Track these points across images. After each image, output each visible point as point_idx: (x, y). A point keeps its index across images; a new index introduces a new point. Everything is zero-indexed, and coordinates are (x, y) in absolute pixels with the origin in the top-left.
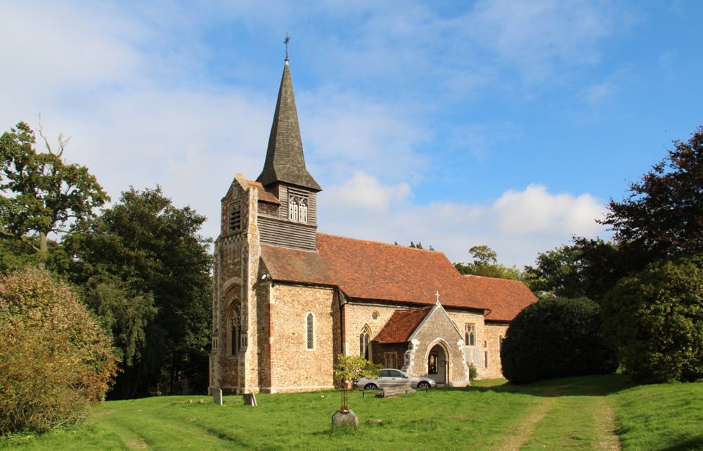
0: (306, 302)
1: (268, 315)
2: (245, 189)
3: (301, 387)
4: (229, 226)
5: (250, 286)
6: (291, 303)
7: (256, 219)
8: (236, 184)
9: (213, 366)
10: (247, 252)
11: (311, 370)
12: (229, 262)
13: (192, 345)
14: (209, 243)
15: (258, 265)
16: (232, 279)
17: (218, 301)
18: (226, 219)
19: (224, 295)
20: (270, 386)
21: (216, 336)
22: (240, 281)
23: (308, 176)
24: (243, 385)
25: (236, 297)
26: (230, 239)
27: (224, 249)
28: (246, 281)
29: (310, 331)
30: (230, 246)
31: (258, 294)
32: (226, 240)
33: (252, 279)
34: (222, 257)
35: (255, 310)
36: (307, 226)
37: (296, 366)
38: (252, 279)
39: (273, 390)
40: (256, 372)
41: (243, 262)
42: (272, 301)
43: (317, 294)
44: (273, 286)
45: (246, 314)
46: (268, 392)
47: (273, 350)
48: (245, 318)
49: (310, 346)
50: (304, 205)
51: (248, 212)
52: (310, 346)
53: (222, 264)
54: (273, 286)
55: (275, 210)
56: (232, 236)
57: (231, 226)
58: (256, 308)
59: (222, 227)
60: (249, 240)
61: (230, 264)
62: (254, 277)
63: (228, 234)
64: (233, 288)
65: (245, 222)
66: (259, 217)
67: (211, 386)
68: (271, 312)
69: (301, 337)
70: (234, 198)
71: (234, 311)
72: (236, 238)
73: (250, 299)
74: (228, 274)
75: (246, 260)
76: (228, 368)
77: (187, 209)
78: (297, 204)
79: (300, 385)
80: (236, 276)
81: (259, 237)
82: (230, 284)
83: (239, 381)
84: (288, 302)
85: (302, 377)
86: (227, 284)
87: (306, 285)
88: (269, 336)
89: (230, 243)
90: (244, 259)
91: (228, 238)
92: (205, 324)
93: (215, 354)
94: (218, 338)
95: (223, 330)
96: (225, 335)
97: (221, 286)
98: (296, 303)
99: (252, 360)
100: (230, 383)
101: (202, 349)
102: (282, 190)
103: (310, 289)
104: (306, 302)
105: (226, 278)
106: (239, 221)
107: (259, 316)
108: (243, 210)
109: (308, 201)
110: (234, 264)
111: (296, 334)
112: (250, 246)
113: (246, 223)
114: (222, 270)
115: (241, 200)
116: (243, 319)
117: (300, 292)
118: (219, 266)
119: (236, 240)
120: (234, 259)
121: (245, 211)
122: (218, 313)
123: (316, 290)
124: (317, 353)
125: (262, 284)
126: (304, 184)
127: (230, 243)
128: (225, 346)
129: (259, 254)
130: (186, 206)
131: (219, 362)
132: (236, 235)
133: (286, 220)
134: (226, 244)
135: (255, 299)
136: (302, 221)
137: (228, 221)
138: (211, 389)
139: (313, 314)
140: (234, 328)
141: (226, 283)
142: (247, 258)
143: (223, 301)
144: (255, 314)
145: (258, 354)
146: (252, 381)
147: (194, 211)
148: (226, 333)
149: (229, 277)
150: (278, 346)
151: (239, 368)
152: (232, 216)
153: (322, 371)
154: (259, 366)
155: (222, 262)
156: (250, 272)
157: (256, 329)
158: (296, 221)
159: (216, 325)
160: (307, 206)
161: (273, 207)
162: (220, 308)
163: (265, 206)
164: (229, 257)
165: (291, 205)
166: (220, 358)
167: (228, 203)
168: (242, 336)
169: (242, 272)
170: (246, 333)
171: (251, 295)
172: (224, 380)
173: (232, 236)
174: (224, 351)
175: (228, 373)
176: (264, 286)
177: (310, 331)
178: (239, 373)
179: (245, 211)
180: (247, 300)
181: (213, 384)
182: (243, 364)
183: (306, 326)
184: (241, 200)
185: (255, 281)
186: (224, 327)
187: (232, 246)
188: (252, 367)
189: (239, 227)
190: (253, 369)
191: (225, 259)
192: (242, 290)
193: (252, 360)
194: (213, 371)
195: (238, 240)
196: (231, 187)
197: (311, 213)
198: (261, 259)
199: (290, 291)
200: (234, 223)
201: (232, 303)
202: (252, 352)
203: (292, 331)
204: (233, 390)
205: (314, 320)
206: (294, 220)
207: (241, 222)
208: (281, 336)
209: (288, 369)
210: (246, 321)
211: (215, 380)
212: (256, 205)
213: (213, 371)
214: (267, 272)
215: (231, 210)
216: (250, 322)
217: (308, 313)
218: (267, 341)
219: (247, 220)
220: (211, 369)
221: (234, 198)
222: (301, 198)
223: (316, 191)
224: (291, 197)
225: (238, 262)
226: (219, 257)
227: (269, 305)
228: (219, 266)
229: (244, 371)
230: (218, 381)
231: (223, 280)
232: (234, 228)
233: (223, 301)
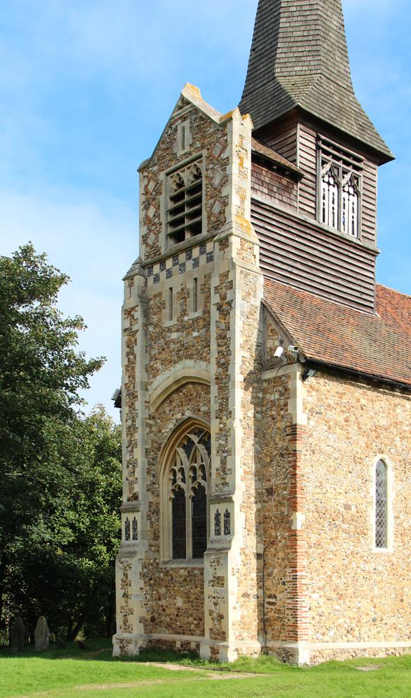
0: (376, 428)
1: (290, 455)
2: (216, 118)
3: (362, 645)
4: (165, 230)
5: (239, 378)
6: (342, 428)
7: (248, 206)
8: (186, 111)
9: (126, 583)
10: (231, 286)
11: (383, 601)
12: (167, 323)
13: (43, 542)
14: (74, 330)
15: (256, 325)
16: (179, 366)
17: (138, 423)
18: (157, 215)
19: (152, 410)
20: (295, 638)
21: (134, 510)
22: (206, 370)
23: (360, 113)
24: (222, 635)
25: (188, 414)
26: (169, 263)
27: (150, 294)
28: (225, 364)
29: (381, 504)
30: (173, 280)
31: (258, 403)
32: (156, 269)
33: (242, 360)
34: (146, 314)
35: (250, 442)
36: (356, 246)
37: (350, 591)
38: (242, 360)
39: (305, 652)
40: (253, 603)
41: (215, 315)
42: (301, 419)
43: (398, 410)
44: (304, 377)
45: (227, 452)
46: (288, 657)
47: (302, 545)
48: (223, 462)
49: (380, 543)
50: (351, 191)
51: (226, 180)
52: (380, 543)
53: (146, 333)
54: (304, 377)
55: (288, 189)
56: (174, 256)
57: (170, 230)
58: (252, 438)
59: (144, 239)
60: (234, 255)
61: (170, 330)
62: (247, 355)
63: (163, 251)
64: (177, 391)
65: (216, 209)
66: (254, 202)
67: (120, 634)
68: (299, 446)
69: (361, 514)
70: (180, 153)
71: (181, 450)
72: (189, 258)
73: (239, 413)
74: (163, 356)
75: (226, 308)
76: (163, 591)
77: (27, 251)
78: (337, 184)
79: (360, 639)
80: (190, 357)
81: (257, 250)
82: (171, 381)
83: (208, 624)
84: (336, 423)
85: (364, 618)
86: (165, 379)
87: (377, 383)
88: (293, 507)
89: (169, 274)
90: (219, 308)
91: (162, 262)
92: (67, 501)
93: (132, 554)
94: (138, 516)
95: (151, 498)
96: (154, 511)
97: (145, 387)
98: (353, 429)
99: (243, 570)
100: (169, 626)
101: (59, 552)
102: (304, 139)
103: (383, 397)
104: (376, 428)
105: (158, 365)
106: (199, 213)
107: (258, 459)
108: (210, 179)
109: (361, 180)
110: (183, 328)
111: (353, 508)
112: (238, 270)
113: (222, 212)
114: (148, 348)
115: (205, 153)
116: (216, 462)
117: (363, 401)
118: (139, 336)
119: (189, 264)
120: (184, 313)
121: (216, 182)
122: (138, 454)
123: (397, 400)
124: (394, 560)
125: (269, 375)
126: (353, 131)
127: (169, 274)
128: (156, 537)
129: (260, 295)
130: (24, 244)
131: (143, 575)
132: (188, 250)
133: (312, 221)
134: (157, 279)
135: (251, 413)
136: (347, 233)
137: (164, 218)
138: (122, 640)
139: (388, 461)
140: (179, 496)
141: (160, 378)
142: (230, 304)
143: (150, 426)
144: (252, 453)
145: (259, 556)
146: (243, 624)
147: (42, 257)
148: (158, 504)
149: (169, 363)
150: (314, 538)
151: (209, 590)
152: (171, 205)
153: (405, 603)
154: (260, 587)
155: (146, 325)
156: (239, 339)
157: (253, 492)
158: (334, 230)
159: (131, 484)
160: (357, 193)
161: (285, 181)
162: (144, 442)
163: (266, 175)
164: (166, 311)
165: (323, 186)
166: (144, 567)
167: (160, 170)
168: (213, 509)
169: (214, 347)
170: (230, 500)
171: (241, 397)
172: (153, 619)
173: (174, 256)
174: (155, 547)
175: (163, 602)
176: (277, 380)
177: (381, 504)
178: (208, 605)
179: (216, 182)
180: (230, 414)
181: (127, 628)
182: (220, 581)
183: (372, 488)
184: (205, 153)
185: (250, 367)
186: (152, 489)
187: (177, 282)
188: (243, 590)
189: (196, 229)
190: (246, 595)
191: (155, 319)
192: (214, 390)
193: (243, 570)
194: (125, 595)
195: (196, 264)
196: (170, 125)
197: (366, 216)
198: (264, 307)
199: (341, 395)
200: (181, 221)
201: (174, 431)
202: (243, 552)
203: (342, 500)
204: (193, 646)
205: (391, 474)
206: (329, 226)
207: (204, 213)
208: (321, 513)
209: (334, 595)
210: (226, 470)
211: (134, 620)
212: (248, 163)
213: (125, 595)
214: (287, 338)
215: (169, 187)
216: (239, 471)
217: (379, 456)
218: (286, 522)
219: (225, 203)
220: (119, 593)
221: (180, 153)
222: (345, 172)
223: (381, 158)
224: (324, 163)
225: (196, 320)
226: (138, 314)
227: (294, 427)
228: (139, 336)
229: (225, 599)
230: (142, 620)
231: (151, 371)
232: (178, 237)
233: (150, 426)
